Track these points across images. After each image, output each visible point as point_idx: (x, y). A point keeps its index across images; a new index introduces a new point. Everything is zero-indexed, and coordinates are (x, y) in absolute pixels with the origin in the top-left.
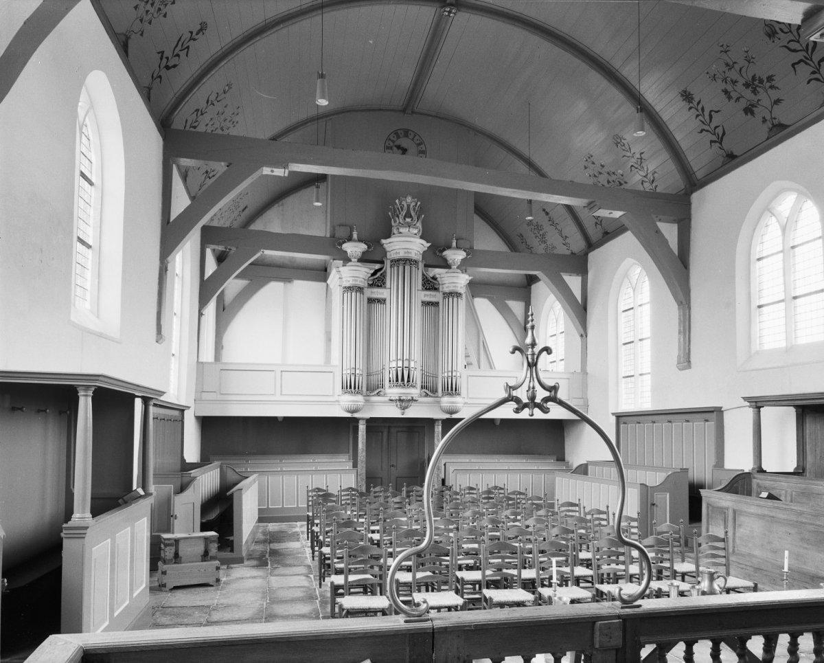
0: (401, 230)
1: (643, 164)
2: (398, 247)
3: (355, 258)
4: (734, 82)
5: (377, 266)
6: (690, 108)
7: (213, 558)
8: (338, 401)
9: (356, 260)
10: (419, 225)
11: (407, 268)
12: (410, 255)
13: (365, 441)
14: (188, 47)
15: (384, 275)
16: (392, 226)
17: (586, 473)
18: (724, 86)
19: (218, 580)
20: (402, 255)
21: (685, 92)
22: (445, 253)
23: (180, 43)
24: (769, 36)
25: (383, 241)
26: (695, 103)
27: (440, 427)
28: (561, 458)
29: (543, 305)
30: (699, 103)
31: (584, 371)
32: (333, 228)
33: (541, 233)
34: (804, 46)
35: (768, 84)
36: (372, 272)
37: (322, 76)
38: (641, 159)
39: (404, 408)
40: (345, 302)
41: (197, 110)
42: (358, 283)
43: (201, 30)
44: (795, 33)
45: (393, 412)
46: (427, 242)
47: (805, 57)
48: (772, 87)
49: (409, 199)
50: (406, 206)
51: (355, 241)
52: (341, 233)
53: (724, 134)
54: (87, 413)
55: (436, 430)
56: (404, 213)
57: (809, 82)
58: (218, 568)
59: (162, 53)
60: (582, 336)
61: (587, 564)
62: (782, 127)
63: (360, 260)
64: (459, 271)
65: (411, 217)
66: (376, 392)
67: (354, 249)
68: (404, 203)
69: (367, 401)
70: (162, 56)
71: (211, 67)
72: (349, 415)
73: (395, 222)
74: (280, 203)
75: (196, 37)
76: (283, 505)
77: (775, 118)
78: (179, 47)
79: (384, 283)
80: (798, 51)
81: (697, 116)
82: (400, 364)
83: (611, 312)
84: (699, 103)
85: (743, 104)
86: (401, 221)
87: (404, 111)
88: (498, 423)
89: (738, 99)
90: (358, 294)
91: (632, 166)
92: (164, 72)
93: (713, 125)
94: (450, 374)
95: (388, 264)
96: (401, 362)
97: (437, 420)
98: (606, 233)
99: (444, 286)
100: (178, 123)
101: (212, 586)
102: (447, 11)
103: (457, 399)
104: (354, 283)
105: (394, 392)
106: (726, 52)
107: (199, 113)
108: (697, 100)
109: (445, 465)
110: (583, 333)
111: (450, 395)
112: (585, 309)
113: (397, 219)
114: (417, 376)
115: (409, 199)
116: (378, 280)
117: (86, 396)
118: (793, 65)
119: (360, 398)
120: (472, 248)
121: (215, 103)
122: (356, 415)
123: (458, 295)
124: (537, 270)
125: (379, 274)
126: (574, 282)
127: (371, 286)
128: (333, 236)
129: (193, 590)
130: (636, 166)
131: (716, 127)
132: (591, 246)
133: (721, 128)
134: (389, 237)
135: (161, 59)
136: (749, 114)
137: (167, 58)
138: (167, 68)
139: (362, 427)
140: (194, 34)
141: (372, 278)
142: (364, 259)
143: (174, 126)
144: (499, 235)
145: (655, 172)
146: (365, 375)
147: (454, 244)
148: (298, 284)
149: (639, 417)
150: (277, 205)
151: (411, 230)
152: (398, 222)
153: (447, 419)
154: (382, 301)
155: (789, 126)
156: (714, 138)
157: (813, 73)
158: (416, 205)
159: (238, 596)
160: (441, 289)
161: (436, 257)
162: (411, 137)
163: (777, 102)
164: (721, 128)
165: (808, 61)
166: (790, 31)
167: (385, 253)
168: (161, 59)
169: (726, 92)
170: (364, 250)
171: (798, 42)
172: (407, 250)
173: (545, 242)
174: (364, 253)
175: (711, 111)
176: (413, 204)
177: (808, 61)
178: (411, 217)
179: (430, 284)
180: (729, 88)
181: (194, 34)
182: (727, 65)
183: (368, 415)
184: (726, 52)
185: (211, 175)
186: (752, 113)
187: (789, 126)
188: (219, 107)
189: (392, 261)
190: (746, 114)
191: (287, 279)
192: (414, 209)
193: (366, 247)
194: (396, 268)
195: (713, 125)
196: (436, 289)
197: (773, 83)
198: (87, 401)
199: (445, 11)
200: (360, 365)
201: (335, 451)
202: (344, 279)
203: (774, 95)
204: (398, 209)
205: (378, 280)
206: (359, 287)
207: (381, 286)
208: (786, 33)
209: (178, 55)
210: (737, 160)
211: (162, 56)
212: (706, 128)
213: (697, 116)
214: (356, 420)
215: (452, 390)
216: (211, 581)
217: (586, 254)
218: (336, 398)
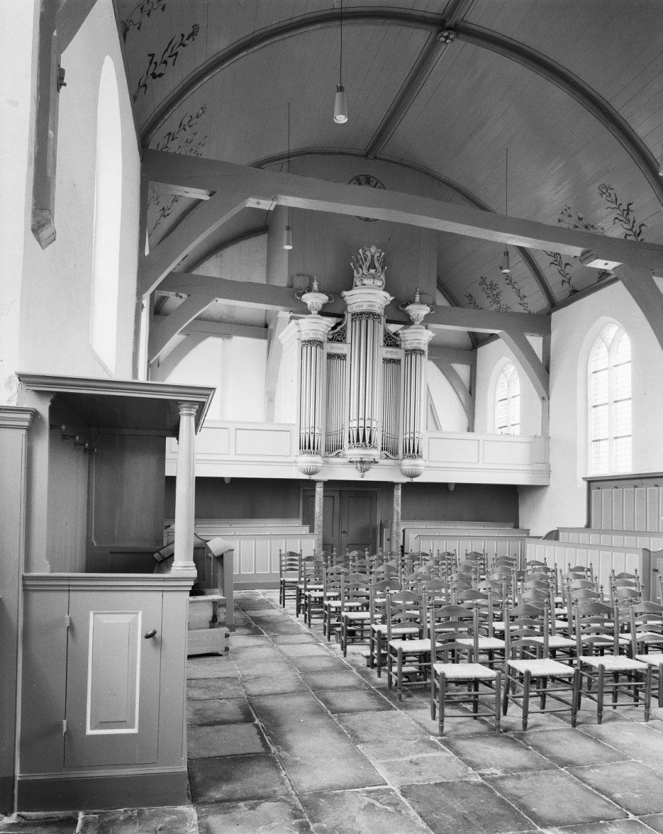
0: (365, 281)
1: (629, 216)
2: (359, 300)
5: (340, 320)
7: (222, 624)
8: (295, 462)
9: (317, 312)
10: (383, 277)
11: (370, 322)
13: (322, 505)
14: (176, 54)
15: (344, 330)
16: (353, 276)
17: (557, 538)
19: (227, 649)
20: (365, 308)
22: (408, 308)
23: (170, 50)
25: (345, 293)
27: (400, 491)
28: (516, 526)
29: (495, 365)
31: (546, 436)
32: (291, 278)
33: (495, 292)
36: (333, 325)
37: (341, 89)
38: (628, 210)
39: (363, 471)
40: (304, 357)
41: (170, 134)
42: (317, 336)
43: (192, 34)
45: (352, 474)
46: (391, 296)
49: (373, 249)
52: (300, 283)
55: (395, 494)
56: (367, 264)
58: (227, 636)
59: (152, 55)
60: (543, 398)
61: (501, 635)
64: (421, 326)
66: (335, 453)
67: (314, 300)
68: (368, 253)
69: (326, 462)
70: (152, 60)
71: (194, 82)
72: (306, 477)
73: (358, 273)
74: (219, 254)
75: (186, 42)
76: (255, 572)
78: (168, 53)
79: (345, 338)
82: (361, 423)
83: (580, 371)
86: (365, 272)
87: (366, 156)
88: (452, 488)
90: (318, 348)
91: (616, 218)
92: (150, 80)
94: (412, 435)
95: (348, 317)
96: (363, 421)
97: (398, 484)
98: (574, 292)
99: (406, 342)
100: (157, 140)
101: (221, 655)
102: (444, 37)
103: (419, 462)
104: (313, 336)
105: (355, 453)
107: (171, 138)
109: (404, 531)
110: (545, 395)
111: (412, 457)
112: (547, 369)
113: (360, 269)
114: (378, 437)
115: (373, 249)
116: (338, 335)
117: (190, 415)
119: (318, 459)
120: (434, 304)
121: (187, 127)
122: (314, 477)
123: (421, 352)
124: (497, 329)
125: (339, 328)
126: (536, 342)
127: (330, 340)
128: (291, 286)
129: (202, 659)
132: (554, 305)
134: (350, 288)
135: (151, 63)
137: (156, 63)
138: (154, 76)
139: (319, 490)
140: (185, 37)
141: (332, 332)
142: (323, 313)
143: (151, 147)
144: (445, 297)
145: (643, 225)
146: (324, 435)
147: (417, 299)
148: (237, 340)
149: (600, 483)
150: (215, 256)
153: (408, 483)
154: (342, 357)
159: (259, 666)
160: (403, 346)
161: (398, 313)
162: (373, 184)
167: (345, 306)
168: (151, 63)
172: (371, 303)
173: (498, 303)
174: (324, 305)
176: (378, 254)
179: (392, 341)
181: (185, 37)
183: (327, 478)
185: (166, 214)
188: (187, 134)
189: (352, 315)
191: (227, 335)
192: (378, 260)
193: (327, 298)
194: (358, 322)
196: (398, 346)
198: (191, 420)
200: (320, 424)
201: (285, 514)
202: (302, 333)
204: (361, 259)
205: (338, 335)
206: (320, 341)
207: (341, 341)
209: (165, 62)
211: (152, 60)
214: (313, 483)
215: (413, 451)
216: (220, 650)
217: (549, 314)
218: (294, 459)
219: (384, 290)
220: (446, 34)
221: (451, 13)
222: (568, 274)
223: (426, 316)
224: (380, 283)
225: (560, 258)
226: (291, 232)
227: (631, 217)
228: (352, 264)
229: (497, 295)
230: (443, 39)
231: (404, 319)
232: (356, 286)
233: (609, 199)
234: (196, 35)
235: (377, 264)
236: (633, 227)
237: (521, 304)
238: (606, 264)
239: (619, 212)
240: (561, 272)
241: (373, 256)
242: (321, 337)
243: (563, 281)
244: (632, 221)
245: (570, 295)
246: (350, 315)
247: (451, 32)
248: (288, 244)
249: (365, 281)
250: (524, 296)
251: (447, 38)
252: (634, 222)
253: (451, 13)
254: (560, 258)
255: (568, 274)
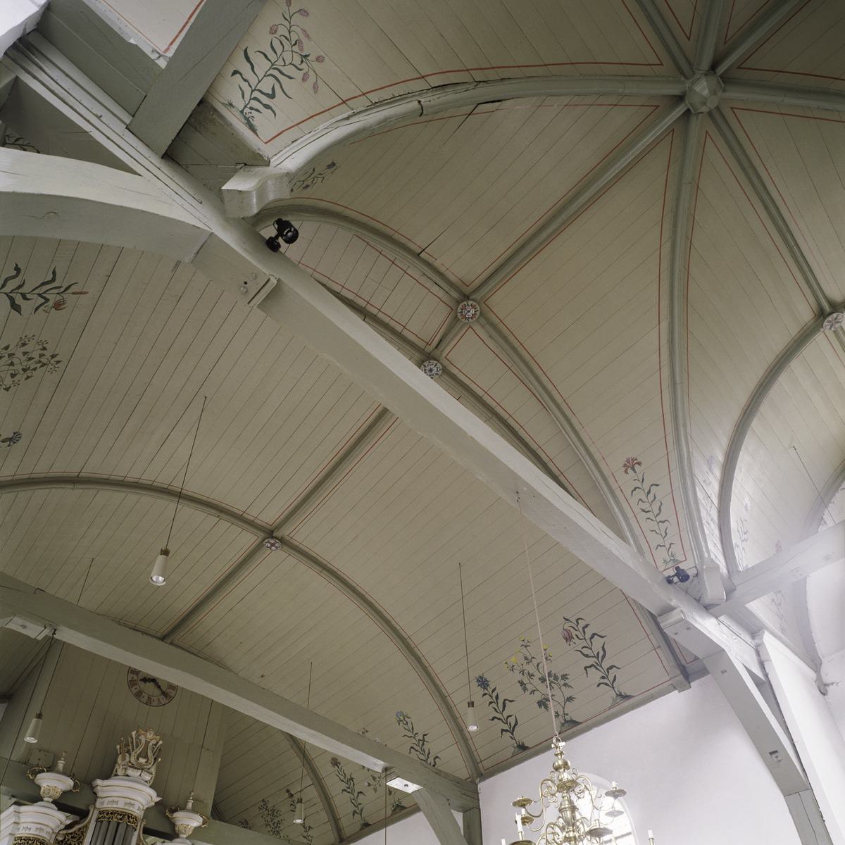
2: (116, 794)
3: (50, 797)
4: (531, 675)
6: (485, 694)
9: (51, 800)
10: (153, 770)
12: (131, 809)
16: (116, 762)
18: (520, 677)
21: (481, 678)
22: (176, 815)
24: (567, 640)
25: (99, 782)
26: (490, 691)
30: (493, 691)
33: (276, 820)
34: (596, 654)
35: (562, 682)
36: (69, 822)
38: (424, 740)
42: (41, 834)
43: (10, 439)
44: (588, 641)
47: (596, 663)
48: (565, 685)
50: (143, 742)
51: (58, 772)
53: (516, 723)
54: (555, 230)
57: (599, 685)
62: (574, 723)
63: (54, 802)
65: (146, 757)
67: (53, 783)
68: (143, 738)
73: (124, 759)
77: (567, 714)
80: (590, 657)
81: (491, 703)
84: (493, 691)
85: (537, 696)
86: (133, 760)
87: (163, 639)
89: (533, 692)
93: (506, 714)
104: (37, 833)
106: (526, 647)
108: (492, 687)
115: (150, 735)
118: (586, 668)
130: (417, 748)
131: (508, 717)
133: (513, 717)
136: (543, 707)
141: (65, 832)
142: (60, 805)
145: (437, 757)
147: (190, 805)
151: (142, 774)
152: (128, 759)
155: (581, 723)
156: (506, 727)
157: (603, 678)
158: (156, 745)
163: (570, 699)
164: (513, 717)
165: (598, 667)
166: (585, 639)
169: (522, 683)
170: (68, 788)
171: (591, 649)
174: (65, 793)
175: (505, 700)
176: (154, 742)
177: (598, 667)
178: (146, 757)
180: (526, 681)
182: (526, 658)
184: (526, 647)
186: (546, 707)
187: (581, 723)
190: (540, 706)
195: (506, 714)
197: (567, 681)
199: (268, 542)
202: (22, 826)
203: (568, 692)
204: (132, 743)
208: (581, 639)
210: (528, 752)
212: (499, 716)
213: (491, 703)
219: (150, 787)
220: (272, 541)
221: (279, 527)
222: (360, 804)
223: (196, 829)
224: (148, 777)
225: (354, 785)
226: (41, 721)
227: (426, 747)
228: (118, 747)
229: (279, 823)
230: (269, 545)
231: (167, 830)
232: (116, 775)
233: (406, 727)
234: (14, 443)
235: (150, 754)
236: (428, 757)
237: (304, 837)
238: (406, 785)
239: (415, 742)
240: (353, 801)
241: (147, 743)
242: (46, 836)
243: (355, 812)
244: (427, 753)
245: (361, 829)
246: (96, 812)
247: (277, 541)
248: (33, 736)
249: (130, 772)
250: (310, 827)
251: (273, 545)
252: (429, 753)
253: (279, 527)
254: (354, 785)
255: (360, 804)
